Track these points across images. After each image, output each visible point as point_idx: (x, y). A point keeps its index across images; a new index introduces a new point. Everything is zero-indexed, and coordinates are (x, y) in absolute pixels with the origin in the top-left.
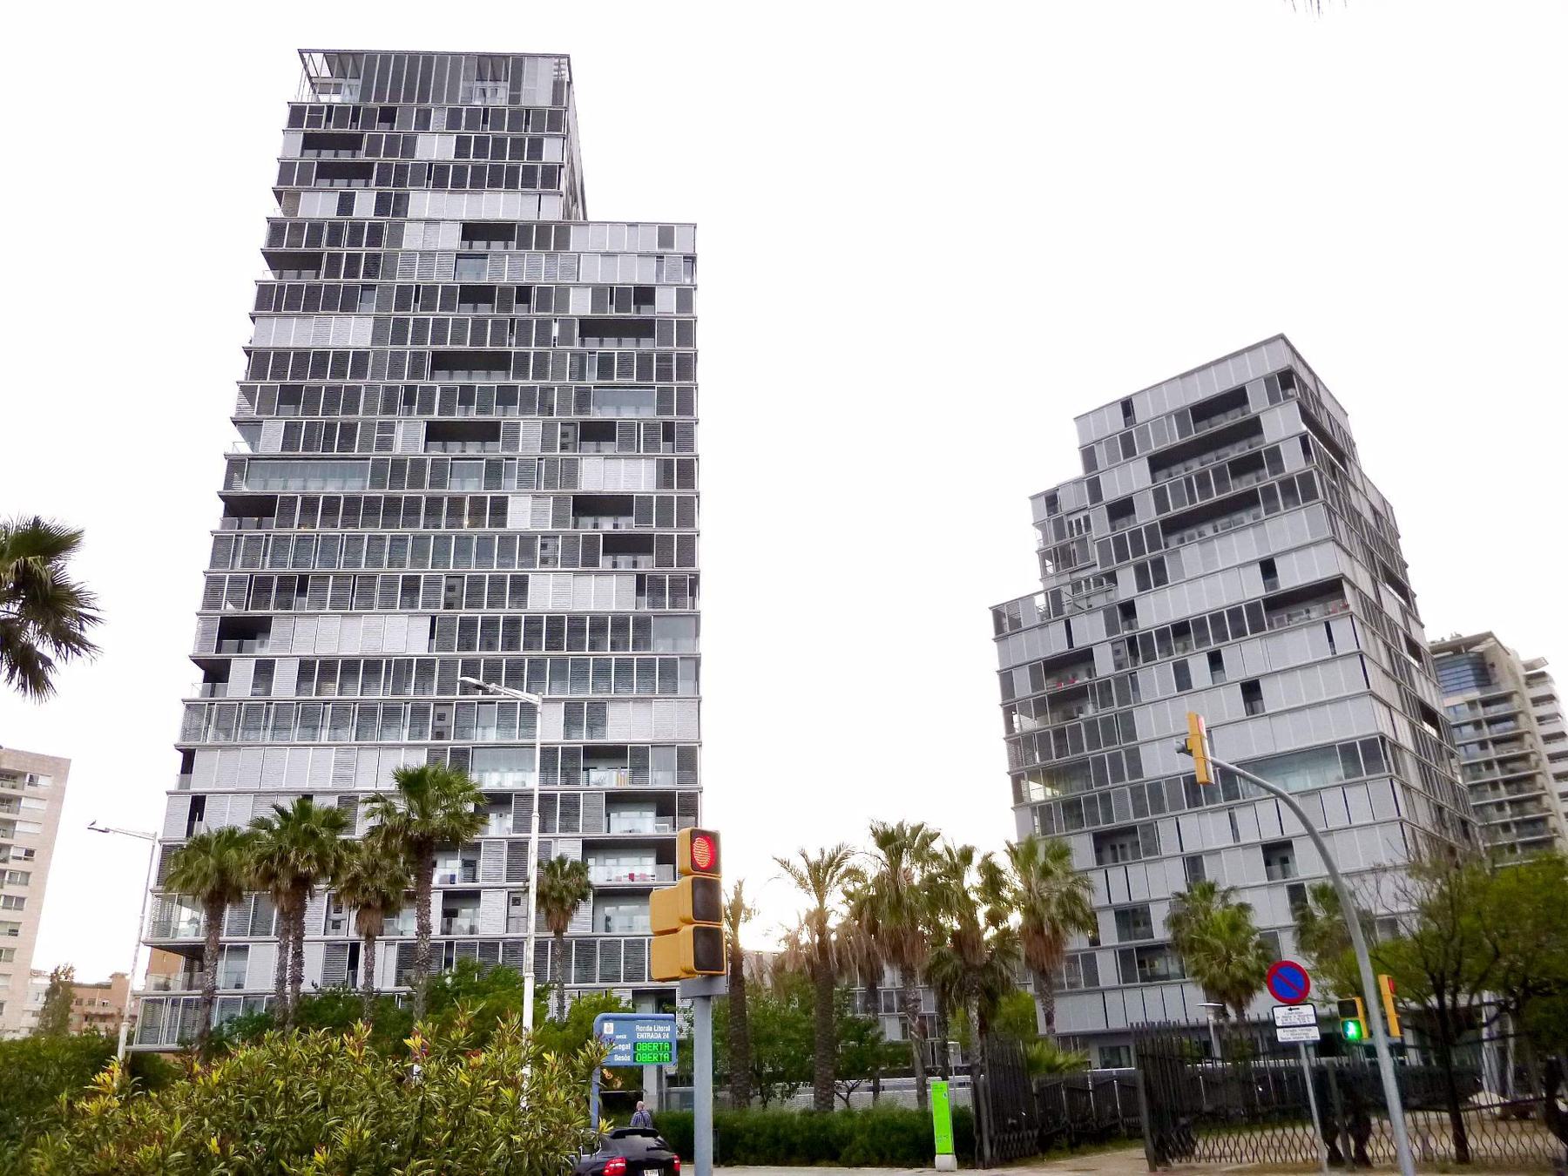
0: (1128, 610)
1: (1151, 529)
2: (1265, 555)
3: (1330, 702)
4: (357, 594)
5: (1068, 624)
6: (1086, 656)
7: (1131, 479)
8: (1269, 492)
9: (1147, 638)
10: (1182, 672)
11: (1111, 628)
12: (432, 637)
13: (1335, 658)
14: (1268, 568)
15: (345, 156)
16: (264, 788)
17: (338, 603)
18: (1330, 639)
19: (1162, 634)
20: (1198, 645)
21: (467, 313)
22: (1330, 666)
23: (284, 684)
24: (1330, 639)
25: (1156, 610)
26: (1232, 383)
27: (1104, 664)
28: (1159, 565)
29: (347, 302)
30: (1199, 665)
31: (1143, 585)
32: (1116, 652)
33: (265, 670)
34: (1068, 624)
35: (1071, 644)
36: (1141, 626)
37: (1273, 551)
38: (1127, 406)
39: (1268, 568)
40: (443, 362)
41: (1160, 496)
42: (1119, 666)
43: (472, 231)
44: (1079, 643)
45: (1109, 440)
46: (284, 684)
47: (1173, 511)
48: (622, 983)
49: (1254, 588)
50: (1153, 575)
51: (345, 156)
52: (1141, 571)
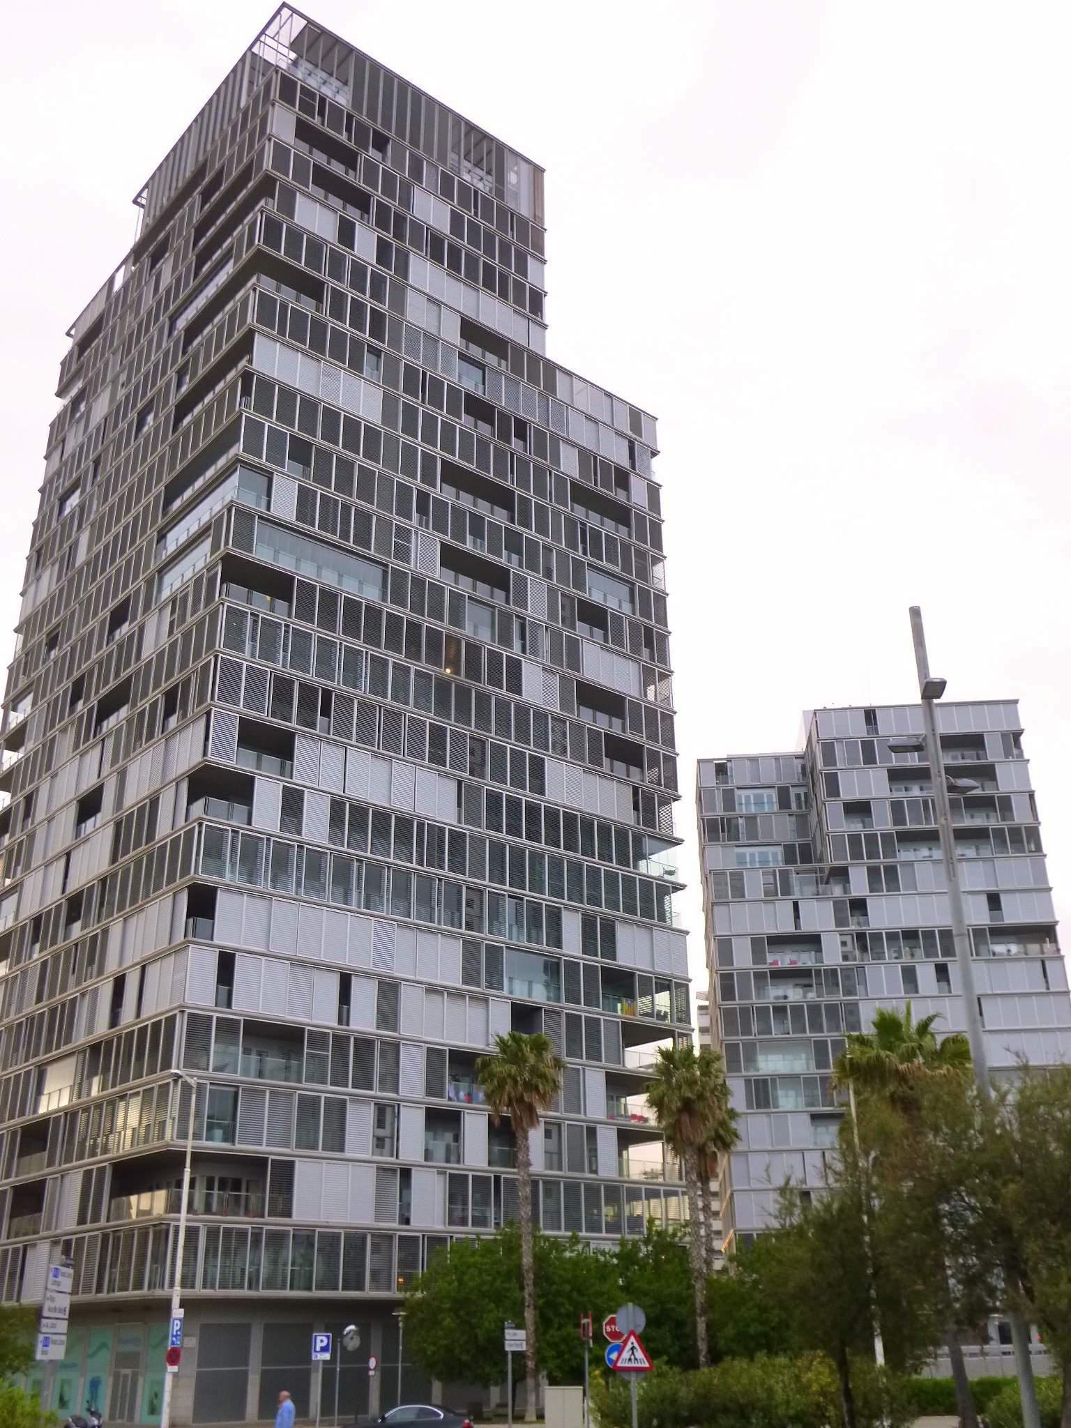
0: (859, 906)
1: (886, 837)
2: (993, 888)
3: (1025, 1031)
4: (384, 733)
5: (796, 905)
6: (813, 941)
7: (868, 784)
8: (999, 833)
9: (877, 937)
10: (910, 976)
11: (841, 922)
12: (459, 805)
13: (1048, 993)
14: (994, 901)
15: (337, 168)
16: (300, 955)
17: (365, 738)
18: (1045, 976)
19: (892, 937)
20: (927, 955)
21: (464, 422)
22: (1045, 999)
23: (315, 826)
24: (1045, 976)
25: (887, 913)
26: (972, 728)
27: (832, 955)
28: (891, 871)
29: (352, 357)
30: (926, 974)
31: (874, 885)
32: (844, 944)
33: (292, 803)
34: (796, 905)
35: (797, 926)
36: (872, 925)
37: (1001, 887)
38: (870, 715)
39: (994, 901)
40: (453, 476)
41: (897, 807)
42: (845, 958)
43: (471, 330)
44: (807, 927)
45: (850, 743)
46: (315, 826)
47: (909, 826)
48: (604, 1235)
49: (978, 914)
50: (886, 879)
51: (337, 168)
52: (873, 872)
